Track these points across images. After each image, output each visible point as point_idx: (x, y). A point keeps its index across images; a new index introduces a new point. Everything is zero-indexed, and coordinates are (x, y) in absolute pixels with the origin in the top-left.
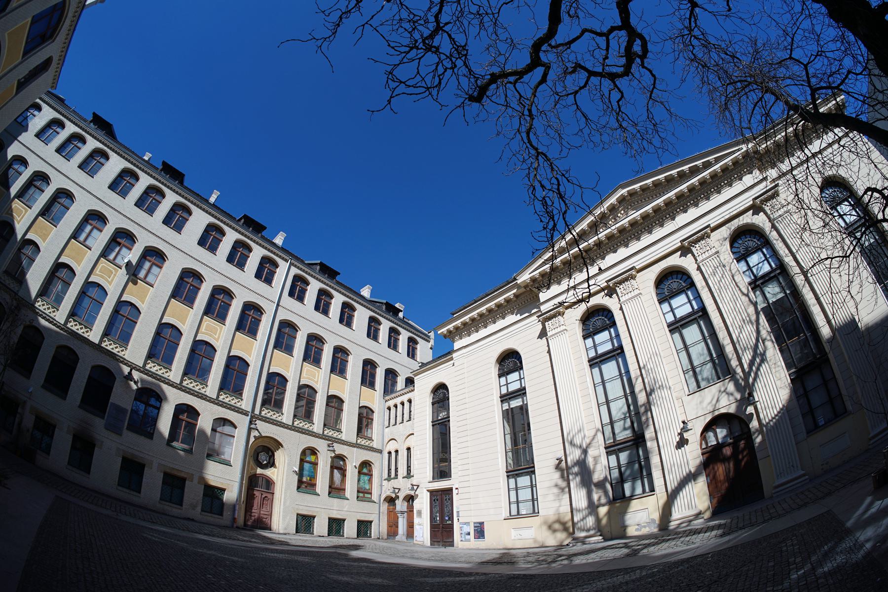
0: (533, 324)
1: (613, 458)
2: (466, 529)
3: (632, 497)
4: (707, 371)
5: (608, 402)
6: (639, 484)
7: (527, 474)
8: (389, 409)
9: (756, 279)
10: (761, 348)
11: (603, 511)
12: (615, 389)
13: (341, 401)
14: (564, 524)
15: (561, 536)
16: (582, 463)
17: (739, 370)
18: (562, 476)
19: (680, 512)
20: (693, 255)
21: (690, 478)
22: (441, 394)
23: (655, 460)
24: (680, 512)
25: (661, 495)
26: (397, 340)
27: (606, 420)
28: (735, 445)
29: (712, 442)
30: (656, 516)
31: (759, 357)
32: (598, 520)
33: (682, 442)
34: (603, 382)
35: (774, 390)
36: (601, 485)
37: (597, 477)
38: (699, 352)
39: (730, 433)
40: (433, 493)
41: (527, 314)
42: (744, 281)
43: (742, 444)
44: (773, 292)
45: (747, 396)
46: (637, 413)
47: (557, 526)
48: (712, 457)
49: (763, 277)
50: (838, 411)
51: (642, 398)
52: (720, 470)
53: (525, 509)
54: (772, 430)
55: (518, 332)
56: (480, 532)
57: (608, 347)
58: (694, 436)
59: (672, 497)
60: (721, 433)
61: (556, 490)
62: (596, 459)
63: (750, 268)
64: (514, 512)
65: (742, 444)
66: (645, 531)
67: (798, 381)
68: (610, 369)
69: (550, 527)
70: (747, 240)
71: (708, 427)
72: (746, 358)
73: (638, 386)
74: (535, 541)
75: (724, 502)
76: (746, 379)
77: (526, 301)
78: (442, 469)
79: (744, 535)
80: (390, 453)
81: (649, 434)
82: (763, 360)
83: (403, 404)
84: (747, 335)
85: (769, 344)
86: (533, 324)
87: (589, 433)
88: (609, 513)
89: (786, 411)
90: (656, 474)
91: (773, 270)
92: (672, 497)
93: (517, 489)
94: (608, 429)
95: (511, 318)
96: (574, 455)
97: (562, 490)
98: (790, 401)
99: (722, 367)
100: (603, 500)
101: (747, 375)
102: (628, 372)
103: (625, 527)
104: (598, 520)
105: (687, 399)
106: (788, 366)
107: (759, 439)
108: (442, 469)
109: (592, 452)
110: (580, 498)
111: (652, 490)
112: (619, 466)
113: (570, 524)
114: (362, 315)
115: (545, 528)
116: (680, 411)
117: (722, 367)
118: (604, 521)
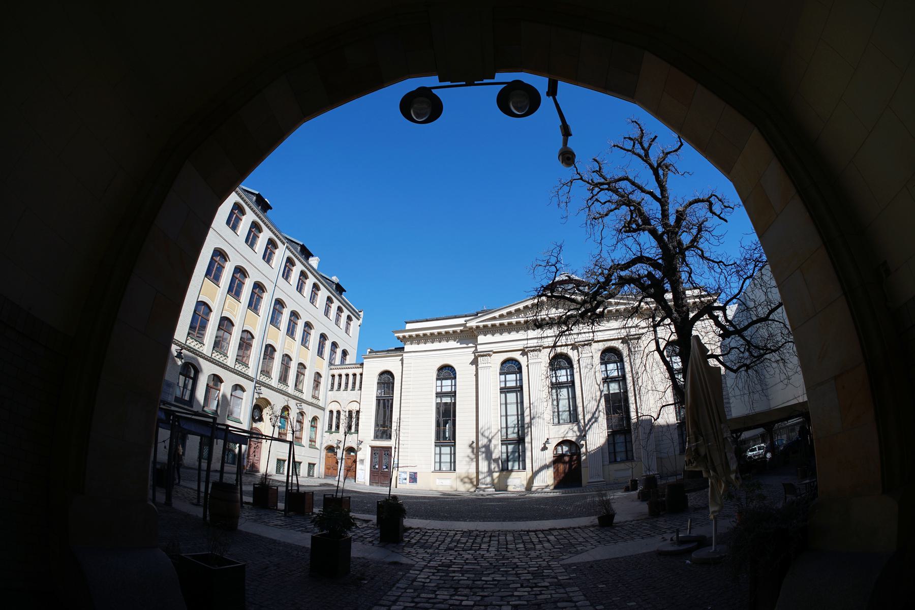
0: (467, 354)
1: (504, 447)
2: (404, 476)
3: (512, 471)
4: (565, 416)
5: (506, 416)
6: (517, 464)
7: (450, 446)
8: (333, 376)
9: (607, 377)
10: (596, 415)
11: (496, 475)
12: (512, 409)
13: (274, 350)
14: (471, 479)
15: (469, 486)
16: (487, 447)
17: (582, 421)
18: (473, 452)
19: (538, 483)
20: (402, 360)
21: (546, 467)
22: (386, 380)
23: (528, 454)
24: (538, 483)
25: (529, 472)
26: (238, 220)
27: (504, 425)
28: (571, 457)
29: (560, 452)
30: (525, 483)
31: (594, 418)
32: (493, 480)
33: (544, 448)
34: (506, 404)
35: (597, 437)
36: (496, 461)
37: (495, 456)
38: (564, 404)
39: (570, 450)
40: (373, 448)
41: (465, 346)
42: (600, 377)
43: (575, 457)
44: (614, 388)
45: (583, 436)
46: (523, 426)
47: (466, 480)
48: (558, 459)
49: (611, 378)
50: (629, 458)
51: (527, 420)
52: (561, 467)
53: (445, 467)
54: (592, 456)
55: (459, 356)
56: (413, 478)
57: (513, 384)
58: (551, 447)
59: (535, 474)
60: (565, 449)
61: (468, 459)
62: (495, 446)
63: (606, 370)
64: (438, 468)
65: (575, 457)
66: (518, 489)
67: (612, 436)
68: (512, 397)
69: (462, 480)
70: (610, 355)
71: (559, 444)
72: (588, 417)
73: (527, 413)
74: (452, 487)
75: (560, 484)
76: (585, 425)
77: (468, 336)
78: (384, 428)
79: (558, 494)
80: (331, 412)
81: (527, 439)
82: (596, 421)
83: (340, 376)
84: (591, 406)
85: (601, 414)
86: (467, 354)
87: (494, 431)
88: (499, 477)
89: (601, 449)
90: (528, 461)
91: (618, 377)
92: (535, 474)
93: (440, 454)
94: (504, 430)
95: (453, 344)
96: (483, 441)
97: (472, 459)
98: (604, 445)
99: (574, 417)
100: (497, 469)
101: (585, 425)
102: (522, 402)
103: (507, 486)
104: (493, 480)
105: (551, 427)
106: (608, 428)
107: (584, 458)
108: (384, 428)
109: (494, 442)
110: (484, 466)
111: (524, 468)
112: (507, 452)
113: (475, 480)
114: (281, 253)
115: (458, 480)
116: (546, 432)
117: (574, 417)
118: (496, 481)
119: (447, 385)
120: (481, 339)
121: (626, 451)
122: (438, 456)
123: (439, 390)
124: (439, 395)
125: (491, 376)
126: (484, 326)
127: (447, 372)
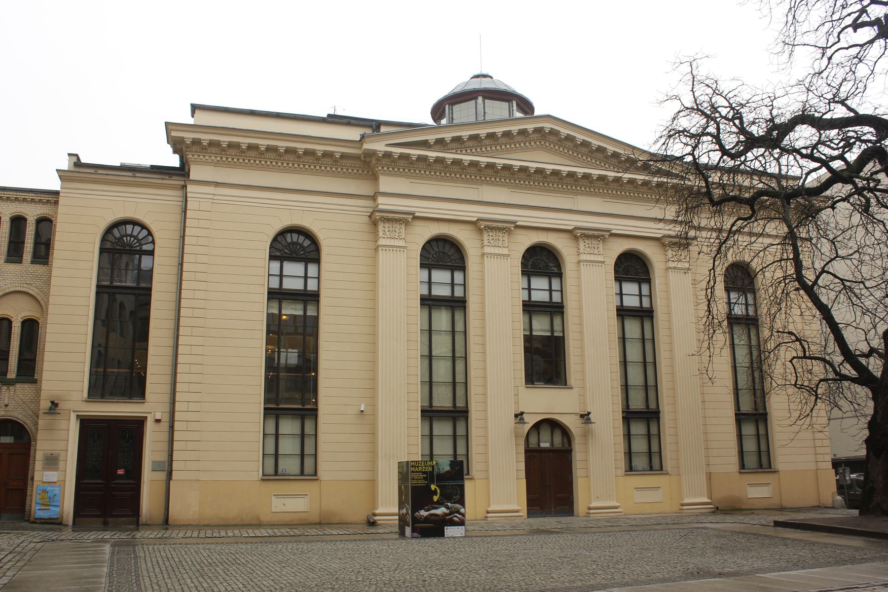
53: (290, 465)
64: (270, 470)
71: (537, 426)
119: (294, 275)
120: (386, 183)
121: (650, 453)
122: (271, 441)
123: (275, 283)
124: (277, 295)
125: (402, 274)
126: (402, 156)
127: (295, 245)
